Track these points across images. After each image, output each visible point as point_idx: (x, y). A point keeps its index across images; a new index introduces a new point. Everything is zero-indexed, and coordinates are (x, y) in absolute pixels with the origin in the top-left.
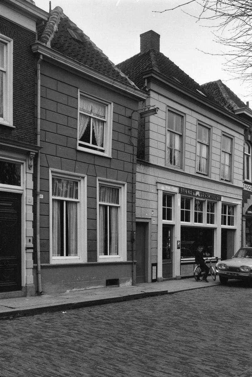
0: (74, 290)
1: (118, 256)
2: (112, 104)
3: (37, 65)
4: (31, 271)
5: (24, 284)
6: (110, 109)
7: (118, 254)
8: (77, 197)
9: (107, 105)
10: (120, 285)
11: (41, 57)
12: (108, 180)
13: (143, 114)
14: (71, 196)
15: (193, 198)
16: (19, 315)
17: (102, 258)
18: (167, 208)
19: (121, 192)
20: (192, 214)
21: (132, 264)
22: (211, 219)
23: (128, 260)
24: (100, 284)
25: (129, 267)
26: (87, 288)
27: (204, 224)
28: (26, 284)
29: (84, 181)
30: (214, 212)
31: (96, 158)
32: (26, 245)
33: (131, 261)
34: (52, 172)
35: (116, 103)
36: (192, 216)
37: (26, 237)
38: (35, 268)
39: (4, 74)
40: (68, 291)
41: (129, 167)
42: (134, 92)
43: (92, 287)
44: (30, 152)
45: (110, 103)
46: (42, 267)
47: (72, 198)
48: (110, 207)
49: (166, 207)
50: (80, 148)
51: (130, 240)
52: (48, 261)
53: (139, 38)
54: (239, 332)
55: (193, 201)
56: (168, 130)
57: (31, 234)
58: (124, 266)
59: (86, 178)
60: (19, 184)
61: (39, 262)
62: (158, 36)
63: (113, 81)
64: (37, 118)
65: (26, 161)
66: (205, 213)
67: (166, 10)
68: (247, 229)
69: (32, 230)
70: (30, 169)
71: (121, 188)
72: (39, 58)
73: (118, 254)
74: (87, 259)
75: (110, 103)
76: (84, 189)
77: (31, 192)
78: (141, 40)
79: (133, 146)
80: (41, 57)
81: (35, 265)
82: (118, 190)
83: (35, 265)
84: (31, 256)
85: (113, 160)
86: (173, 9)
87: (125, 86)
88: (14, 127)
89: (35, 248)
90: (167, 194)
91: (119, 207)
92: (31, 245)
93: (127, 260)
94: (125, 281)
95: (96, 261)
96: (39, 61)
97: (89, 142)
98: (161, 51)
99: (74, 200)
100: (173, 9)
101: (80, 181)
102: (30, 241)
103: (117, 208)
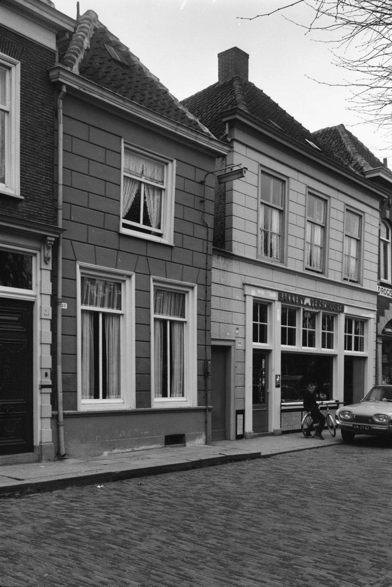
0: (116, 451)
1: (183, 399)
2: (175, 161)
3: (57, 101)
4: (48, 422)
5: (37, 442)
6: (172, 169)
7: (183, 396)
8: (119, 307)
9: (167, 164)
10: (187, 444)
11: (64, 89)
12: (168, 280)
13: (222, 178)
14: (110, 306)
15: (300, 308)
16: (29, 490)
17: (158, 402)
18: (260, 325)
19: (188, 299)
20: (299, 333)
21: (205, 410)
22: (328, 342)
23: (199, 405)
24: (155, 443)
25: (200, 416)
26: (136, 449)
27: (318, 349)
28: (41, 442)
29: (131, 281)
30: (333, 331)
31: (150, 246)
32: (41, 382)
33: (204, 407)
34: (81, 267)
35: (180, 161)
36: (299, 336)
37: (41, 368)
38: (55, 418)
39: (6, 115)
40: (106, 453)
41: (200, 260)
42: (208, 143)
43: (143, 447)
44: (47, 236)
45: (172, 161)
46: (66, 416)
47: (113, 308)
48: (172, 322)
49: (259, 323)
50: (125, 231)
51: (202, 373)
52: (75, 406)
53: (217, 59)
54: (371, 517)
55: (299, 314)
56: (261, 203)
57: (49, 364)
58: (193, 415)
59: (133, 278)
60: (29, 287)
61: (61, 407)
62: (246, 56)
63: (175, 126)
64: (57, 183)
65: (40, 251)
66: (319, 331)
67: (258, 16)
68: (384, 356)
69: (50, 357)
70: (46, 263)
71: (187, 292)
72: (60, 91)
73: (183, 396)
74: (135, 404)
75: (172, 161)
76: (131, 294)
77: (48, 299)
78: (219, 63)
79: (207, 227)
80: (64, 89)
81: (55, 412)
82: (184, 295)
83: (55, 412)
84: (48, 398)
85: (176, 250)
86: (269, 14)
87: (195, 135)
88: (22, 197)
89: (54, 386)
90: (259, 303)
91: (186, 322)
92: (49, 381)
93: (198, 406)
94: (194, 438)
95: (150, 406)
96: (61, 94)
97: (139, 222)
98: (251, 79)
99: (115, 311)
100: (269, 14)
101: (124, 281)
102: (46, 375)
103: (182, 323)
